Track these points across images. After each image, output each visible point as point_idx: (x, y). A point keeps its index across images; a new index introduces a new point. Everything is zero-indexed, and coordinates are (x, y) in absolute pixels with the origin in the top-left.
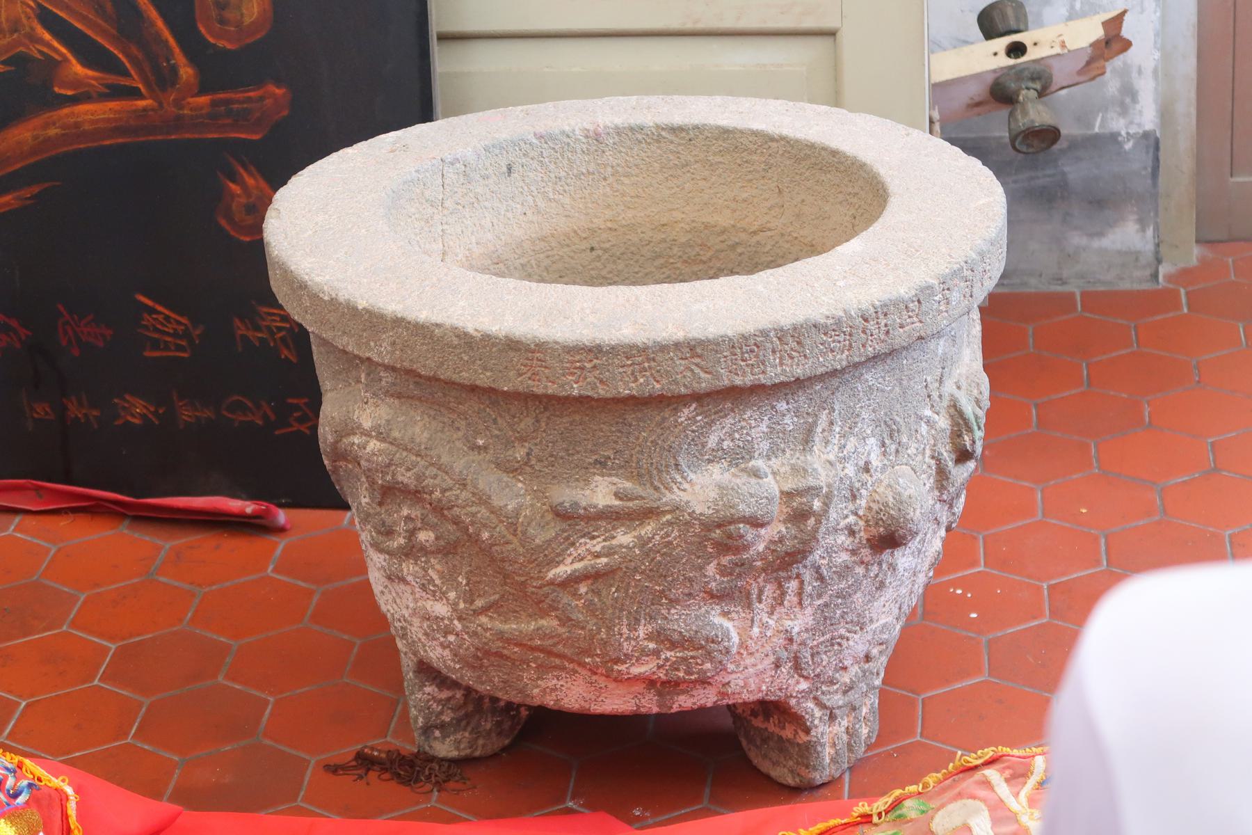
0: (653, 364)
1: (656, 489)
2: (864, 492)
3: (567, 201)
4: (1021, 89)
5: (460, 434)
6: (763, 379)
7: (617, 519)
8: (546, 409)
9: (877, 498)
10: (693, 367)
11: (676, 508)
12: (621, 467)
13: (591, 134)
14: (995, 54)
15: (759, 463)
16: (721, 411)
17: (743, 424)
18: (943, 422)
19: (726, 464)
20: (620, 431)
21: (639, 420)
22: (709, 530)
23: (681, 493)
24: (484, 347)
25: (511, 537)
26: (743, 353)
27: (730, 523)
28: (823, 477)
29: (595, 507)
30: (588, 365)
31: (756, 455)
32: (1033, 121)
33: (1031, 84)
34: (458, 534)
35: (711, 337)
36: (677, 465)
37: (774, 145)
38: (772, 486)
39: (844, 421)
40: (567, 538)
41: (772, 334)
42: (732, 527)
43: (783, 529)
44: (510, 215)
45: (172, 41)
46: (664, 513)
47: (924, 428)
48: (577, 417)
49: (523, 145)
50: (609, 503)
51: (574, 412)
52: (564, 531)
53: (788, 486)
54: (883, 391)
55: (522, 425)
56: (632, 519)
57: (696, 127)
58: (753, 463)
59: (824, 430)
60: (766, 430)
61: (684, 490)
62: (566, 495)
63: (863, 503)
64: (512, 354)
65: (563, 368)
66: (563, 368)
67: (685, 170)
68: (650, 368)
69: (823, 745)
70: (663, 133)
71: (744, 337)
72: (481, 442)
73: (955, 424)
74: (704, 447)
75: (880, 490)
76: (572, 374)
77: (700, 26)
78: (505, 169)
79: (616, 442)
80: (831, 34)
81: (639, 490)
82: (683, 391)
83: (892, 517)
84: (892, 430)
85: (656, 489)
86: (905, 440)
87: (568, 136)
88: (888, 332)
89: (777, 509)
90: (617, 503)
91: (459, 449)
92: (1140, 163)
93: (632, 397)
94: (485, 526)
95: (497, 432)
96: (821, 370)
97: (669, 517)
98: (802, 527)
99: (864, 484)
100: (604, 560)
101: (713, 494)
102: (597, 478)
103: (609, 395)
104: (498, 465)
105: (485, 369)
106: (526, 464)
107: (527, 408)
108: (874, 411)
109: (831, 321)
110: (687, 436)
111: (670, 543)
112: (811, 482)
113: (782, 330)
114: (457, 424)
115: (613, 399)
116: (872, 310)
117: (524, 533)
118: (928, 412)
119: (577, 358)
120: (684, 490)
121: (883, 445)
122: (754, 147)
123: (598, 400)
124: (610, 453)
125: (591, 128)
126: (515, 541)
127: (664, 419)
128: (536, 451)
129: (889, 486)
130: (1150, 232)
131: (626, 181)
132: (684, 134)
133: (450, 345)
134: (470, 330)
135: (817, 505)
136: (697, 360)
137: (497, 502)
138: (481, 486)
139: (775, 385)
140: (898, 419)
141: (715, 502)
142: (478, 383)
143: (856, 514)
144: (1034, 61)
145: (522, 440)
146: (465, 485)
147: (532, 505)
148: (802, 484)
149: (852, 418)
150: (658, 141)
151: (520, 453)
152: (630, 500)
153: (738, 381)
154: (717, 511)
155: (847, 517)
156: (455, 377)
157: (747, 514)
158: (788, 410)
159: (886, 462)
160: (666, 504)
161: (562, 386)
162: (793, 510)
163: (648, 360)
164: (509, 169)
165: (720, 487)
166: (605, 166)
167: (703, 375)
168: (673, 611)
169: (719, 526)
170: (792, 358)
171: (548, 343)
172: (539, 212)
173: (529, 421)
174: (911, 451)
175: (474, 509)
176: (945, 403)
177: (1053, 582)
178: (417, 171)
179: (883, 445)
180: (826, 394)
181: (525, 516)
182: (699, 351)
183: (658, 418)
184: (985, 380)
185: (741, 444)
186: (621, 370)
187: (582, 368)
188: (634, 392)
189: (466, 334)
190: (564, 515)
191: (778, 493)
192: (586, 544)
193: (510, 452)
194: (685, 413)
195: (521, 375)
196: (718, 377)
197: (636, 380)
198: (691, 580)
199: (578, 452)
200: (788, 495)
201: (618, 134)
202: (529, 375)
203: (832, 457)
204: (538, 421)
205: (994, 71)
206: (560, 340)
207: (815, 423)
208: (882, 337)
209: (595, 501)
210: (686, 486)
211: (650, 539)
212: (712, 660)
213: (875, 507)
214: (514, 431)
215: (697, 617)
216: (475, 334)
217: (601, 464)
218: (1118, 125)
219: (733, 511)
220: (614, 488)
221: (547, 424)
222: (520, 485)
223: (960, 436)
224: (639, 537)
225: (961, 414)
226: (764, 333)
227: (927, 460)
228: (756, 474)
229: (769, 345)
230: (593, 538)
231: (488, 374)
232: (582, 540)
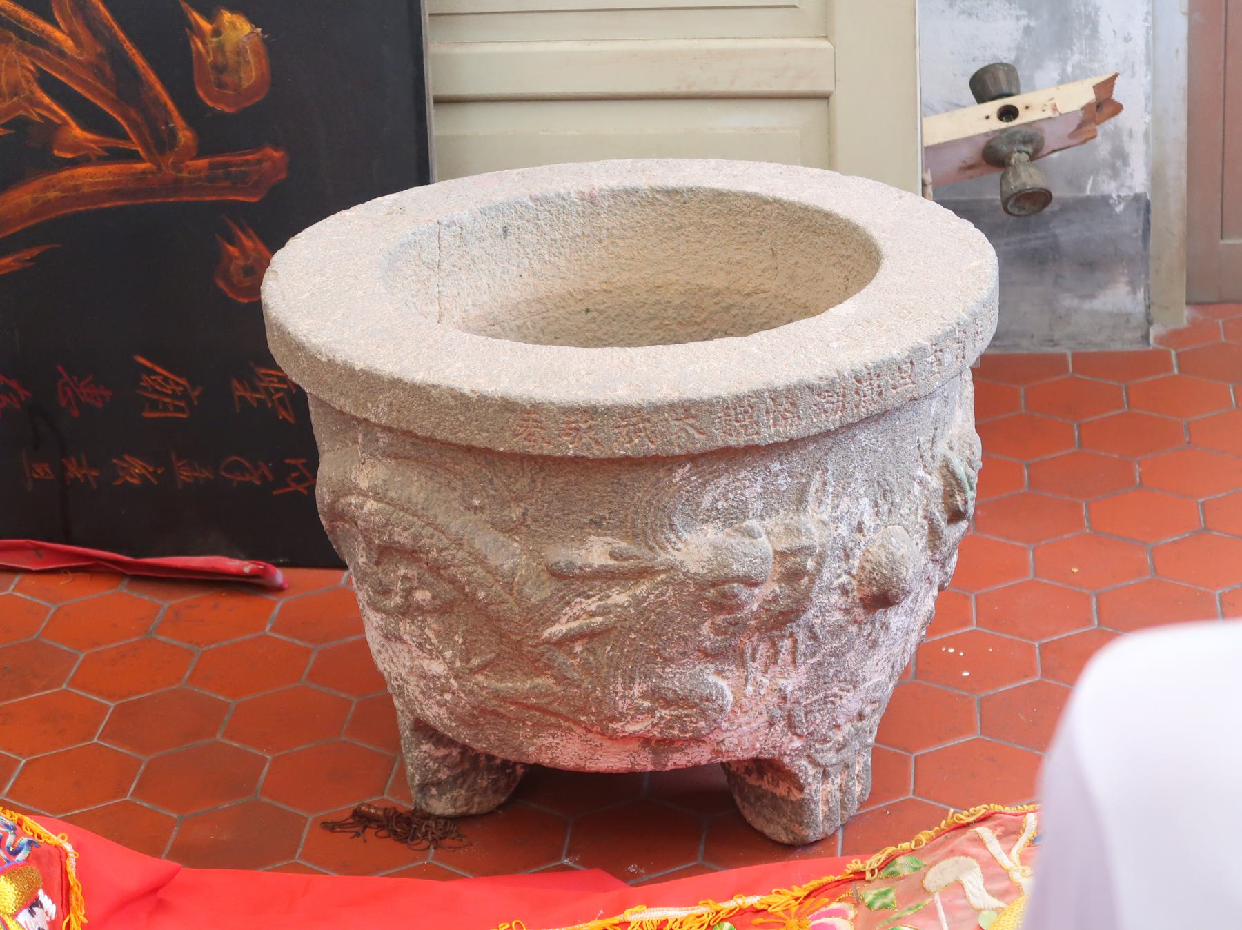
0: (648, 425)
1: (651, 548)
2: (857, 551)
3: (562, 262)
4: (1012, 152)
5: (457, 494)
6: (757, 440)
7: (613, 578)
8: (541, 469)
9: (870, 557)
11: (671, 568)
12: (616, 527)
13: (587, 197)
14: (987, 117)
15: (753, 523)
16: (715, 471)
17: (737, 484)
18: (936, 483)
19: (720, 524)
21: (634, 480)
22: (704, 590)
23: (676, 553)
24: (481, 408)
25: (507, 596)
26: (737, 414)
27: (724, 582)
30: (584, 426)
32: (1024, 184)
33: (1022, 148)
34: (455, 593)
35: (705, 397)
36: (671, 525)
37: (768, 207)
38: (765, 546)
40: (563, 598)
42: (726, 587)
44: (506, 277)
45: (170, 105)
46: (659, 572)
47: (916, 489)
48: (573, 478)
49: (518, 207)
50: (604, 563)
52: (559, 590)
53: (781, 546)
55: (518, 486)
56: (627, 579)
57: (691, 190)
58: (747, 523)
59: (817, 491)
61: (679, 550)
62: (561, 554)
63: (856, 562)
64: (508, 415)
65: (558, 429)
66: (558, 429)
67: (679, 232)
68: (645, 428)
69: (816, 803)
70: (658, 196)
71: (739, 398)
72: (477, 502)
73: (947, 484)
74: (698, 507)
76: (568, 435)
77: (695, 90)
78: (501, 231)
79: (611, 502)
80: (825, 97)
81: (634, 550)
83: (885, 577)
84: (885, 491)
85: (651, 548)
86: (897, 500)
87: (563, 199)
88: (881, 393)
89: (771, 569)
90: (612, 562)
91: (455, 509)
92: (1131, 225)
94: (481, 585)
95: (493, 492)
96: (814, 431)
97: (663, 576)
98: (796, 586)
99: (857, 544)
100: (599, 619)
101: (707, 554)
102: (593, 538)
103: (604, 456)
104: (494, 525)
105: (481, 429)
106: (522, 524)
107: (523, 469)
108: (867, 471)
109: (825, 382)
110: (681, 496)
111: (665, 602)
112: (805, 541)
113: (775, 391)
114: (453, 485)
115: (608, 459)
116: (865, 371)
117: (520, 592)
118: (920, 473)
119: (573, 419)
120: (679, 550)
121: (876, 505)
123: (593, 461)
124: (606, 513)
125: (587, 190)
126: (511, 600)
127: (659, 479)
128: (532, 510)
129: (882, 545)
130: (1141, 294)
131: (621, 243)
132: (678, 197)
134: (466, 391)
135: (810, 564)
136: (692, 421)
137: (493, 561)
138: (477, 546)
140: (891, 479)
141: (709, 561)
142: (474, 443)
143: (849, 574)
144: (1026, 124)
145: (518, 500)
146: (461, 545)
147: (528, 565)
148: (795, 543)
149: (845, 479)
150: (653, 204)
151: (516, 513)
152: (625, 559)
153: (732, 442)
154: (712, 571)
155: (840, 576)
156: (452, 438)
157: (741, 574)
158: (782, 471)
159: (879, 522)
160: (661, 564)
161: (558, 446)
162: (787, 570)
163: (643, 421)
164: (505, 231)
166: (600, 228)
167: (697, 436)
168: (668, 670)
169: (713, 585)
170: (786, 419)
171: (543, 403)
172: (534, 274)
174: (904, 511)
175: (470, 569)
176: (938, 463)
177: (1044, 641)
178: (414, 234)
179: (876, 505)
180: (819, 454)
182: (693, 411)
183: (653, 479)
185: (735, 504)
186: (616, 431)
187: (578, 429)
189: (462, 395)
190: (560, 575)
192: (581, 603)
193: (506, 513)
194: (680, 474)
195: (517, 436)
196: (712, 437)
197: (631, 441)
198: (685, 639)
200: (782, 555)
201: (613, 196)
202: (525, 435)
203: (825, 517)
204: (533, 481)
205: (986, 134)
206: (555, 401)
207: (808, 483)
208: (875, 398)
210: (680, 545)
211: (645, 599)
212: (706, 718)
213: (868, 566)
214: (510, 491)
215: (691, 676)
216: (471, 395)
217: (597, 524)
218: (1109, 187)
219: (727, 571)
220: (609, 548)
222: (516, 545)
223: (952, 496)
224: (634, 597)
225: (953, 474)
226: (758, 394)
227: (920, 520)
228: (750, 534)
229: (763, 406)
230: (588, 597)
231: (484, 435)
232: (578, 600)
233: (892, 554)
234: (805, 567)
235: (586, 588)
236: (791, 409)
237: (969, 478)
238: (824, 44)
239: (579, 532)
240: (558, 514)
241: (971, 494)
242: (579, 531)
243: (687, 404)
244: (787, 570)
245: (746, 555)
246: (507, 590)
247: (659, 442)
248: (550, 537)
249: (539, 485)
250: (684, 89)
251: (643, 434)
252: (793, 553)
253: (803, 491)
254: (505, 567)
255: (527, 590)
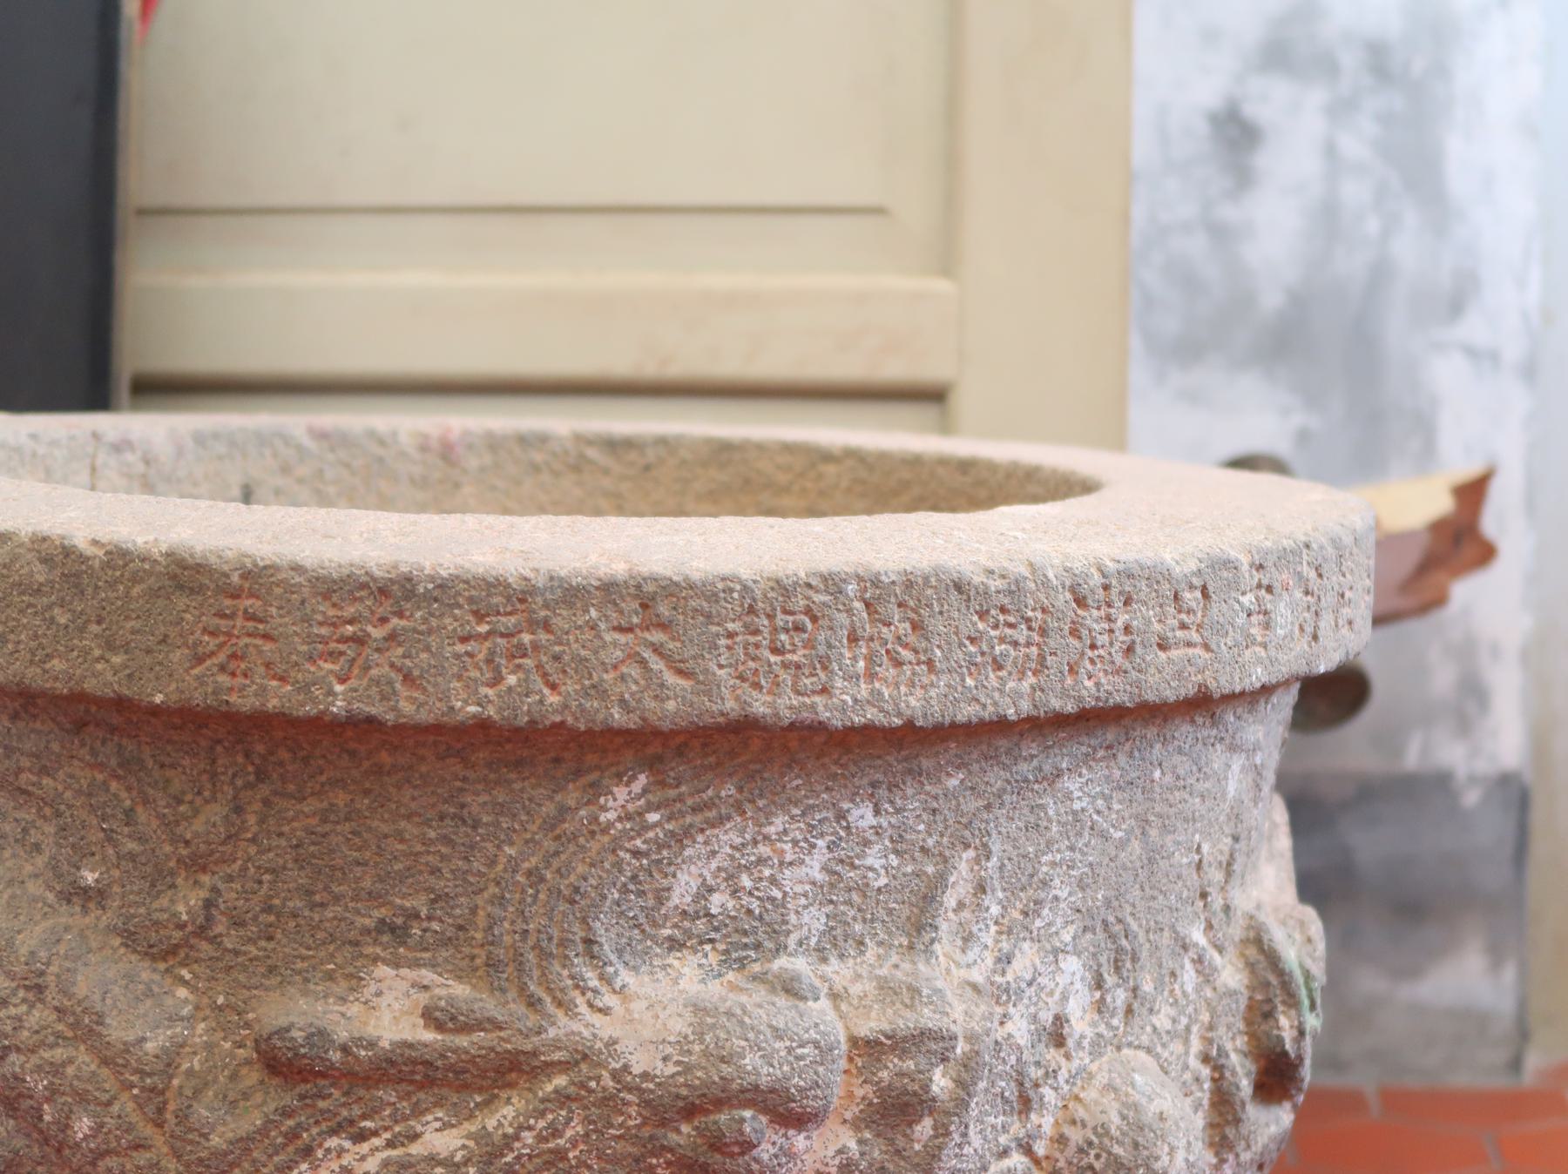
0: (543, 637)
1: (533, 1003)
5: (40, 861)
6: (826, 711)
7: (428, 1083)
8: (261, 776)
9: (1081, 1113)
10: (647, 654)
11: (582, 1057)
12: (447, 942)
15: (800, 964)
16: (709, 805)
17: (764, 850)
18: (1232, 976)
19: (713, 959)
20: (446, 840)
21: (500, 809)
22: (663, 1123)
23: (596, 1019)
24: (112, 585)
25: (149, 1131)
27: (719, 1104)
28: (958, 1015)
29: (372, 1044)
30: (377, 633)
31: (792, 941)
34: (19, 1142)
35: (696, 576)
36: (589, 942)
37: (830, 469)
39: (1012, 890)
40: (292, 1136)
41: (851, 588)
42: (723, 1118)
43: (853, 1145)
46: (550, 1068)
47: (1189, 976)
48: (341, 799)
51: (339, 783)
52: (287, 1113)
53: (868, 1027)
54: (1105, 837)
55: (198, 825)
56: (465, 1087)
58: (781, 962)
59: (961, 905)
60: (819, 877)
61: (605, 1011)
62: (296, 1011)
63: (1045, 1122)
64: (181, 601)
65: (310, 639)
66: (310, 639)
68: (536, 647)
71: (784, 589)
72: (90, 877)
73: (1258, 984)
74: (660, 901)
75: (1090, 1095)
76: (333, 656)
79: (435, 871)
81: (489, 1006)
82: (617, 717)
84: (1120, 950)
86: (1147, 987)
88: (1129, 650)
89: (840, 1087)
90: (429, 1036)
91: (35, 900)
92: (1492, 830)
93: (483, 725)
94: (82, 1098)
95: (132, 846)
96: (967, 712)
97: (561, 1081)
98: (901, 1142)
101: (679, 1025)
102: (383, 971)
103: (424, 717)
104: (130, 938)
105: (110, 646)
106: (202, 931)
107: (214, 776)
108: (1082, 887)
110: (618, 865)
111: (560, 1154)
112: (928, 1018)
113: (876, 582)
114: (34, 836)
115: (437, 729)
116: (1097, 580)
117: (182, 1116)
119: (350, 611)
120: (605, 1011)
121: (1099, 984)
122: (783, 478)
123: (399, 728)
124: (420, 903)
126: (159, 1140)
127: (563, 811)
128: (230, 895)
129: (1110, 1087)
130: (1509, 974)
132: (633, 456)
133: (24, 587)
134: (80, 541)
135: (941, 1082)
136: (657, 636)
137: (117, 1031)
138: (81, 990)
139: (851, 730)
140: (1134, 926)
141: (683, 1043)
142: (90, 685)
143: (1028, 1151)
145: (197, 864)
146: (40, 989)
147: (209, 1047)
148: (906, 1021)
149: (1029, 892)
150: (576, 469)
151: (186, 902)
152: (466, 1029)
153: (760, 705)
154: (688, 1069)
155: (1004, 1153)
156: (34, 677)
157: (764, 1081)
158: (878, 831)
159: (1102, 1029)
160: (556, 1045)
161: (305, 688)
162: (881, 1091)
163: (533, 625)
165: (698, 1009)
167: (670, 678)
169: (690, 1111)
170: (898, 663)
171: (273, 568)
173: (216, 812)
174: (1162, 1021)
175: (59, 1054)
176: (1236, 931)
179: (1099, 984)
180: (971, 804)
181: (190, 1073)
182: (664, 609)
183: (549, 809)
184: (1310, 913)
185: (755, 905)
186: (460, 648)
187: (359, 640)
188: (491, 711)
189: (68, 552)
190: (288, 1066)
191: (842, 1039)
192: (341, 1152)
193: (164, 902)
194: (620, 798)
195: (200, 660)
196: (708, 687)
197: (497, 680)
199: (337, 899)
200: (868, 1049)
202: (221, 657)
203: (977, 976)
204: (239, 810)
206: (308, 564)
208: (1119, 659)
209: (371, 1031)
211: (509, 1141)
213: (1075, 1136)
214: (175, 840)
216: (90, 551)
217: (395, 931)
218: (1452, 755)
219: (727, 1070)
220: (423, 998)
221: (262, 821)
222: (182, 993)
223: (1269, 1015)
224: (481, 1136)
225: (1273, 959)
226: (832, 583)
227: (1194, 1062)
228: (790, 987)
229: (842, 618)
230: (361, 1137)
231: (117, 660)
232: (333, 1142)
233: (1136, 1107)
234: (926, 1088)
235: (357, 1111)
236: (912, 639)
237: (1308, 975)
238: (942, 285)
239: (347, 957)
240: (296, 903)
241: (1312, 1022)
242: (348, 951)
243: (650, 588)
244: (881, 1091)
245: (778, 1034)
246: (150, 1110)
247: (570, 687)
248: (272, 970)
249: (252, 820)
250: (650, 370)
251: (528, 662)
252: (900, 1044)
253: (928, 898)
254: (150, 1046)
255: (202, 1112)
